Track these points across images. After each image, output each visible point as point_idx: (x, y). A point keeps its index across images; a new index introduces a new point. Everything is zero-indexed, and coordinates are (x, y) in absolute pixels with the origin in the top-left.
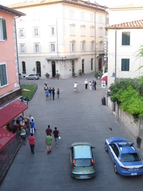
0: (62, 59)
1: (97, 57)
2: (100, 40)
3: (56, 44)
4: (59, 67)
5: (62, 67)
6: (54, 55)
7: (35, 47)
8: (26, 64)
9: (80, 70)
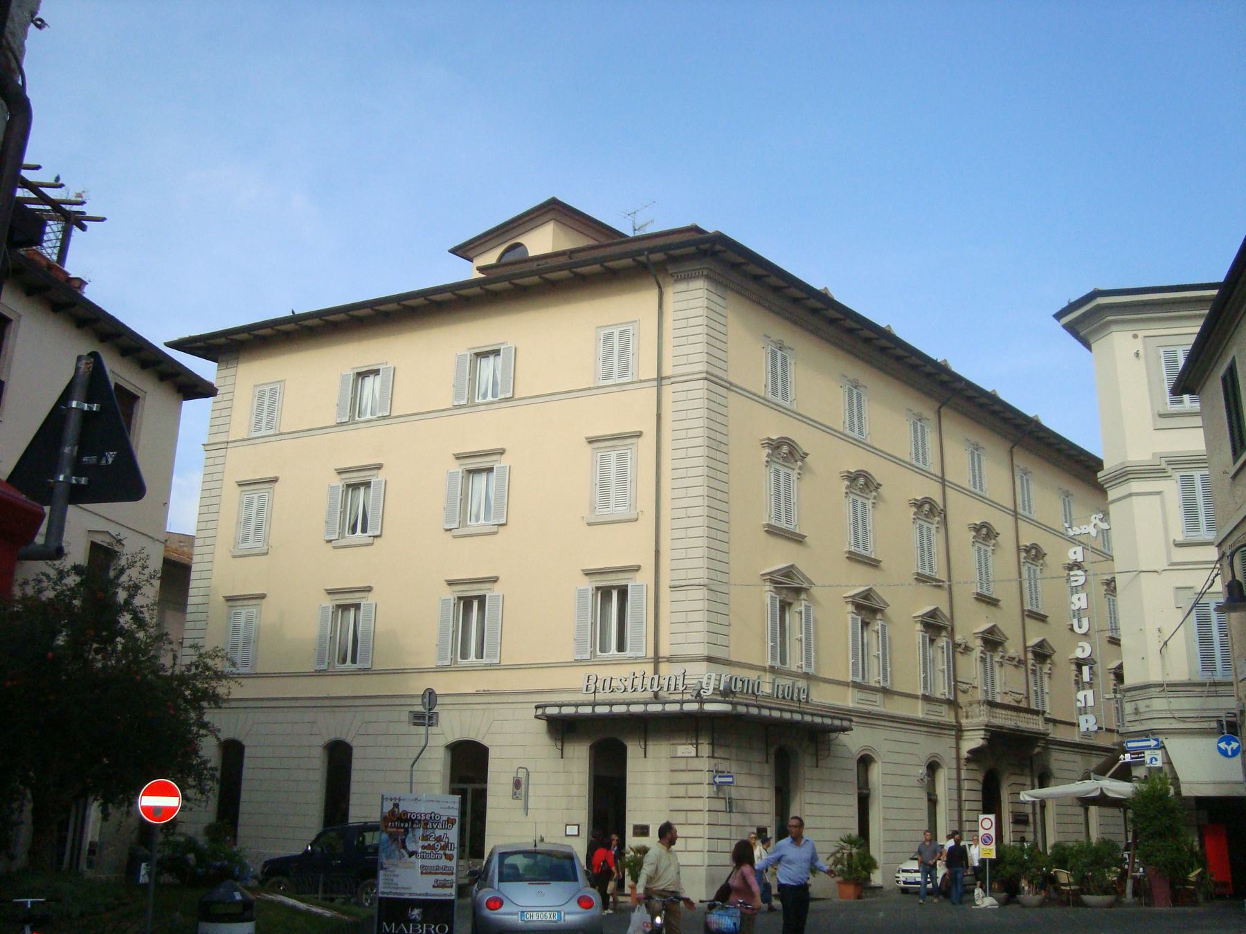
0: (694, 707)
1: (975, 754)
2: (986, 626)
3: (640, 584)
4: (658, 783)
5: (693, 790)
6: (622, 684)
7: (451, 613)
8: (354, 787)
9: (850, 841)
